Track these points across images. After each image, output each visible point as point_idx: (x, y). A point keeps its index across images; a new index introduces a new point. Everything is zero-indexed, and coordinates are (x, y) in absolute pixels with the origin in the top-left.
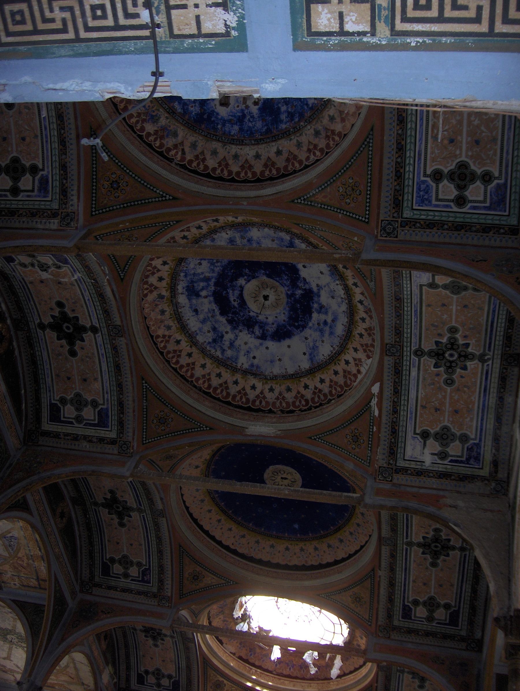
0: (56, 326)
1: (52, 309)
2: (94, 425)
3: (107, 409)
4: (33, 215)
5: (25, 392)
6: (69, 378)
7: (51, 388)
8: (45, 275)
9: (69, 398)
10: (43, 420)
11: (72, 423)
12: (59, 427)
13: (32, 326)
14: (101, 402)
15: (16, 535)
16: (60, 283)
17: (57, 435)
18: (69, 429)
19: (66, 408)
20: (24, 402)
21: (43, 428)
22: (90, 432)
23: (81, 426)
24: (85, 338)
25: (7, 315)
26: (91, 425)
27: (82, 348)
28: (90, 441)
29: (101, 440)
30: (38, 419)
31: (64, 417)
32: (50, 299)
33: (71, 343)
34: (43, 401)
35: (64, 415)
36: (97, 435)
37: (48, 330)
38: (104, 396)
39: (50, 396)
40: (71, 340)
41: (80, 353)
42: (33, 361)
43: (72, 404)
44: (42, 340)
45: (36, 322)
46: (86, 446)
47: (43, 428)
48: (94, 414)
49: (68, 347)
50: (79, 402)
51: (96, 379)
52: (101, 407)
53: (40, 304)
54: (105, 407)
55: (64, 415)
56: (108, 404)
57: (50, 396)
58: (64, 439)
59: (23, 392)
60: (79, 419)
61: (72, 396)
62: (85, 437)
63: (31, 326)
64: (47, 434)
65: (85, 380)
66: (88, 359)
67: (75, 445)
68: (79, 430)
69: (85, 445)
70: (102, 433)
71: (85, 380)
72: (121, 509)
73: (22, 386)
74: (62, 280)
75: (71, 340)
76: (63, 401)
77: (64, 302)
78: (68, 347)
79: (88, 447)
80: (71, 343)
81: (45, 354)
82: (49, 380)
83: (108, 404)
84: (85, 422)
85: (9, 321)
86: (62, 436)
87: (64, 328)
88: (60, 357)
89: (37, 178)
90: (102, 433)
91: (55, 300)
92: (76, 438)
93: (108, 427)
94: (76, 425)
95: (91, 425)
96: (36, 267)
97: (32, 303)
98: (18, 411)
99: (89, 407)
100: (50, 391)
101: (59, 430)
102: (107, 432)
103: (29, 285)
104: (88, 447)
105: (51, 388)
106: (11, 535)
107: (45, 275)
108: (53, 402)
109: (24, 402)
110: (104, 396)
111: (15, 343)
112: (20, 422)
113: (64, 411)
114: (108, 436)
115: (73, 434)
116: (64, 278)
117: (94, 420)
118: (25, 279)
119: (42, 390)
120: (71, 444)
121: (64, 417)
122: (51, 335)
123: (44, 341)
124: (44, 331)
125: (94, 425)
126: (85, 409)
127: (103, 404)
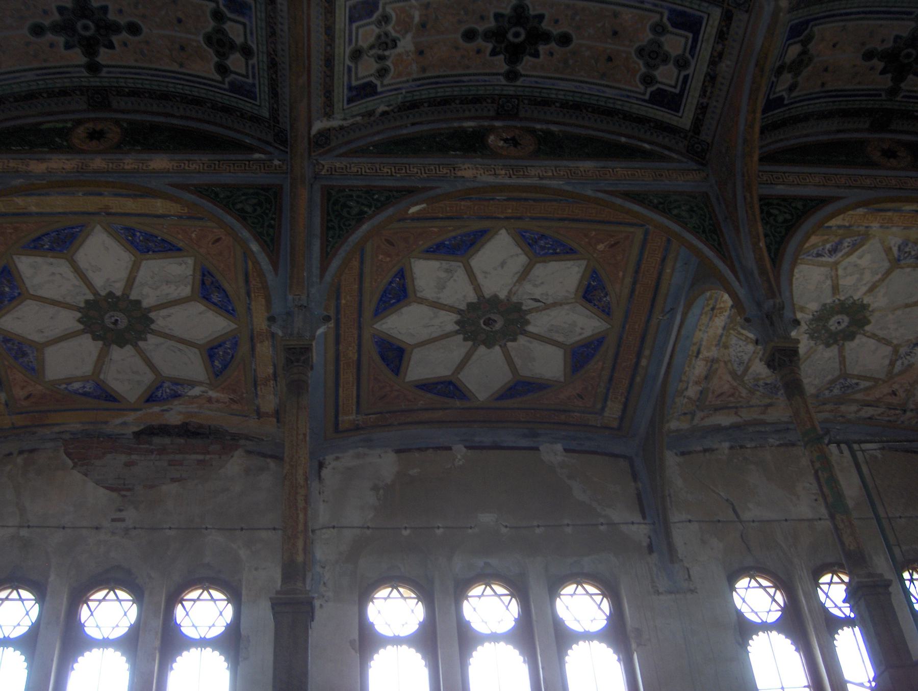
0: (514, 53)
1: (479, 52)
2: (695, 41)
3: (672, 11)
4: (273, 34)
5: (650, 143)
6: (610, 59)
7: (624, 93)
8: (406, 44)
9: (643, 69)
10: (675, 123)
11: (686, 78)
12: (689, 100)
13: (511, 91)
14: (657, 18)
15: (899, 241)
16: (423, 25)
17: (702, 109)
18: (696, 86)
19: (659, 79)
20: (640, 143)
21: (688, 128)
22: (706, 50)
23: (693, 63)
24: (536, 13)
25: (486, 124)
26: (693, 47)
27: (556, 22)
28: (721, 55)
29: (721, 36)
30: (672, 130)
31: (675, 87)
32: (457, 48)
33: (546, 37)
34: (643, 113)
35: (671, 86)
36: (712, 40)
37: (520, 68)
38: (646, 10)
39: (637, 99)
40: (537, 36)
41: (565, 28)
42: (577, 107)
43: (655, 67)
44: (536, 82)
45: (504, 82)
46: (727, 66)
47: (688, 128)
48: (676, 34)
49: (553, 45)
50: (653, 55)
51: (616, 15)
52: (665, 20)
53: (468, 67)
54: (666, 14)
55: (671, 86)
56: (662, 6)
57: (637, 99)
58: (710, 98)
59: (623, 139)
60: (682, 63)
61: (641, 63)
62: (714, 61)
63: (511, 93)
64: (697, 123)
65: (615, 33)
66: (578, 18)
67: (722, 84)
68: (699, 69)
69: (725, 66)
70: (710, 28)
71: (615, 33)
72: (79, 25)
73: (614, 137)
74: (417, 19)
75: (537, 36)
76: (648, 80)
77: (463, 28)
78: (553, 45)
79: (729, 63)
80: (546, 37)
81: (562, 85)
82: (610, 93)
83: (662, 6)
84: (687, 55)
85: (497, 124)
86: (705, 101)
87: (910, 50)
88: (571, 62)
89: (229, 15)
90: (710, 28)
91: (461, 41)
92: (711, 78)
93: (701, 18)
94: (690, 71)
95: (693, 47)
96: (387, 53)
97: (465, 79)
98: (646, 155)
99: (663, 39)
100: (628, 97)
101: (695, 102)
102: (711, 22)
103: (428, 74)
104: (729, 63)
105: (624, 93)
106: (895, 250)
107: (406, 44)
108: (647, 97)
109: (640, 143)
110: (646, 10)
111: (538, 126)
112: (663, 158)
113: (664, 84)
114: (716, 23)
115: (704, 81)
116: (412, 18)
117: (687, 38)
118: (415, 76)
119: (626, 108)
120: (720, 90)
121: (675, 87)
122: (526, 65)
123: (539, 80)
124: (521, 75)
125: (695, 41)
126: (666, 47)
127: (662, 14)
